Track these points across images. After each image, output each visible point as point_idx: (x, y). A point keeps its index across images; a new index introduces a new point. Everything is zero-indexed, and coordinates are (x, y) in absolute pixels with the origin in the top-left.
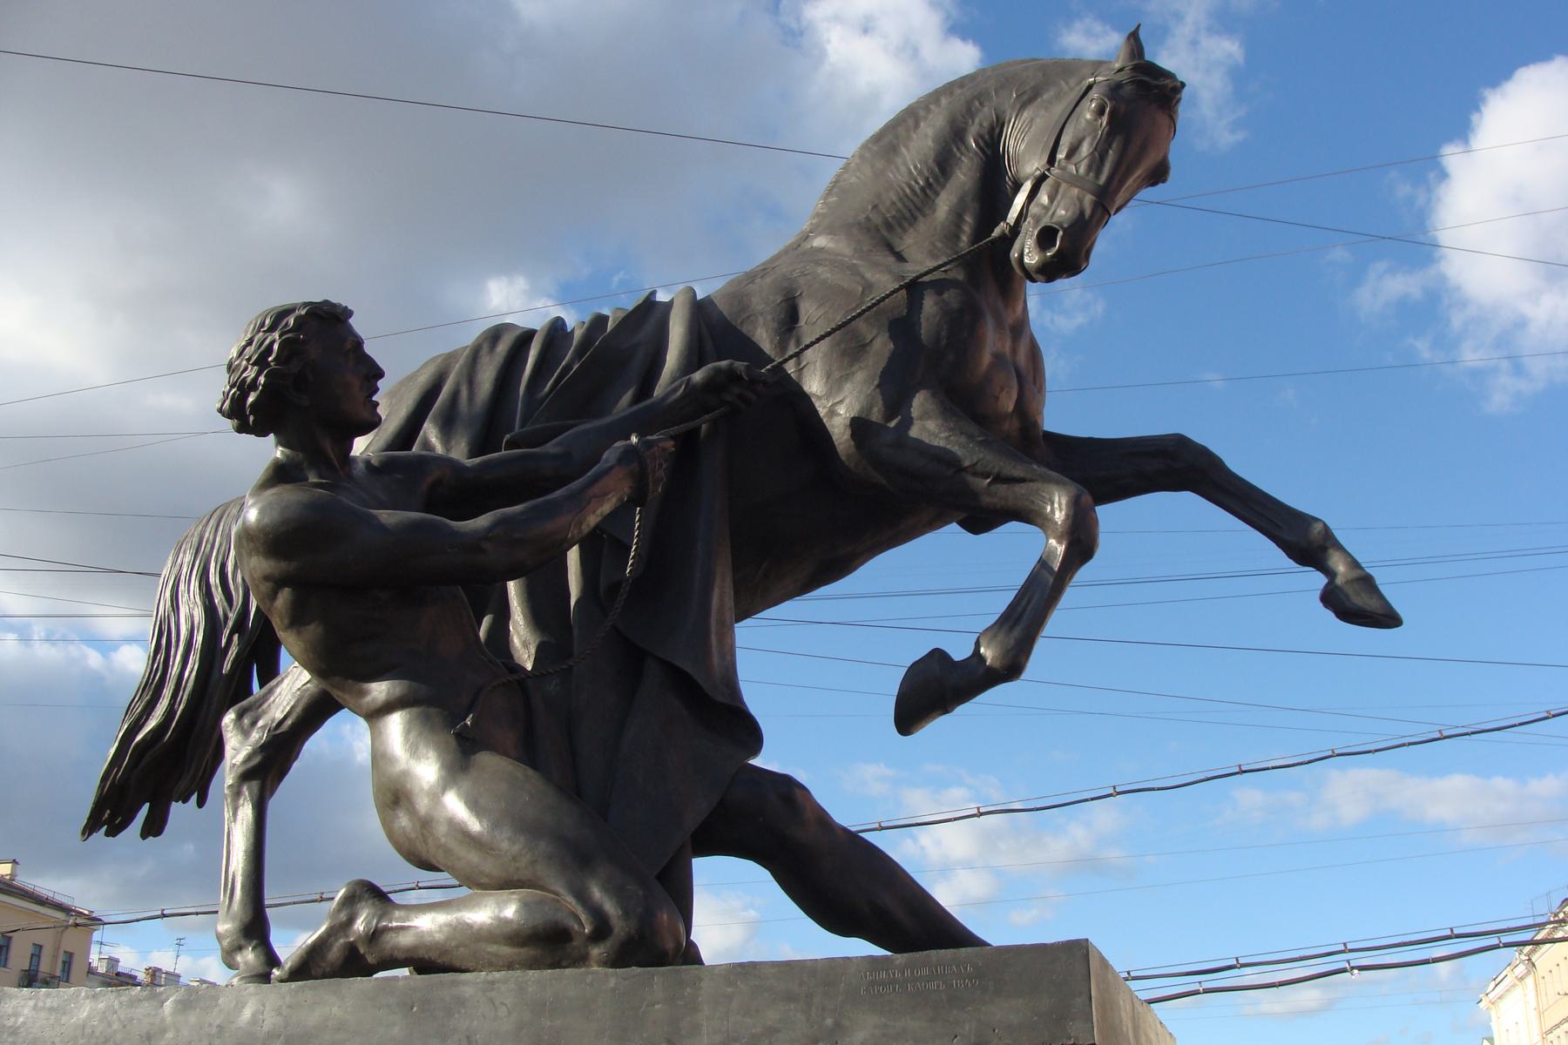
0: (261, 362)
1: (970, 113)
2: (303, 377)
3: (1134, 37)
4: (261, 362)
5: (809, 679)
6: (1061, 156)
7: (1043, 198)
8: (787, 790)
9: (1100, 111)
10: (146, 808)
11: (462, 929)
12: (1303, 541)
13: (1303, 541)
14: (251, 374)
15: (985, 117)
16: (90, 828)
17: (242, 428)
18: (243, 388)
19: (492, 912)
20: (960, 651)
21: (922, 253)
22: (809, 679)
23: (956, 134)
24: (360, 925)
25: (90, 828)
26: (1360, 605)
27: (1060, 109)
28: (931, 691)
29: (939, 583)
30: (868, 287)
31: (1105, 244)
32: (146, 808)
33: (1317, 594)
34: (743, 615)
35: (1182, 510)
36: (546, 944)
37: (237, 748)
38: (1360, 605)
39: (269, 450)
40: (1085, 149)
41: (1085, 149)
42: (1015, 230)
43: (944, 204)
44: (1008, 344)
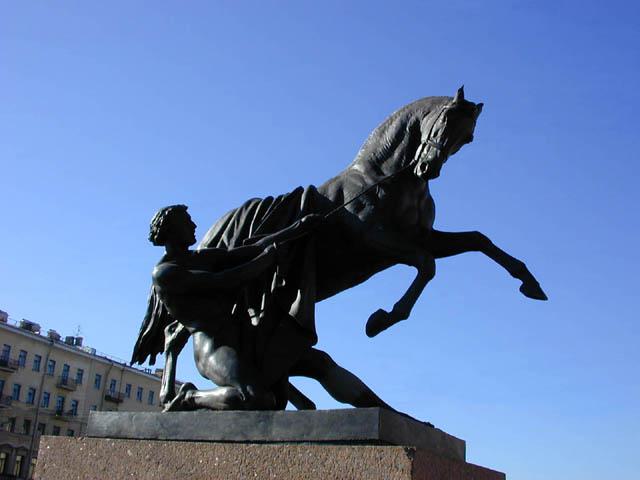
0: (158, 226)
1: (408, 118)
2: (174, 228)
3: (461, 91)
4: (158, 226)
5: (339, 323)
6: (432, 135)
7: (425, 151)
8: (323, 356)
9: (444, 121)
10: (149, 357)
11: (213, 397)
12: (516, 268)
13: (516, 268)
14: (155, 229)
15: (413, 118)
16: (482, 105)
17: (155, 245)
18: (154, 234)
19: (223, 392)
20: (389, 309)
21: (387, 169)
22: (339, 323)
23: (403, 126)
24: (187, 396)
25: (482, 105)
26: (532, 289)
27: (435, 116)
28: (378, 323)
29: (389, 284)
30: (365, 184)
31: (445, 168)
32: (149, 357)
33: (194, 383)
34: (318, 301)
35: (476, 258)
36: (232, 403)
37: (169, 339)
38: (532, 289)
39: (162, 251)
40: (440, 134)
41: (440, 134)
42: (417, 162)
43: (396, 154)
44: (416, 202)
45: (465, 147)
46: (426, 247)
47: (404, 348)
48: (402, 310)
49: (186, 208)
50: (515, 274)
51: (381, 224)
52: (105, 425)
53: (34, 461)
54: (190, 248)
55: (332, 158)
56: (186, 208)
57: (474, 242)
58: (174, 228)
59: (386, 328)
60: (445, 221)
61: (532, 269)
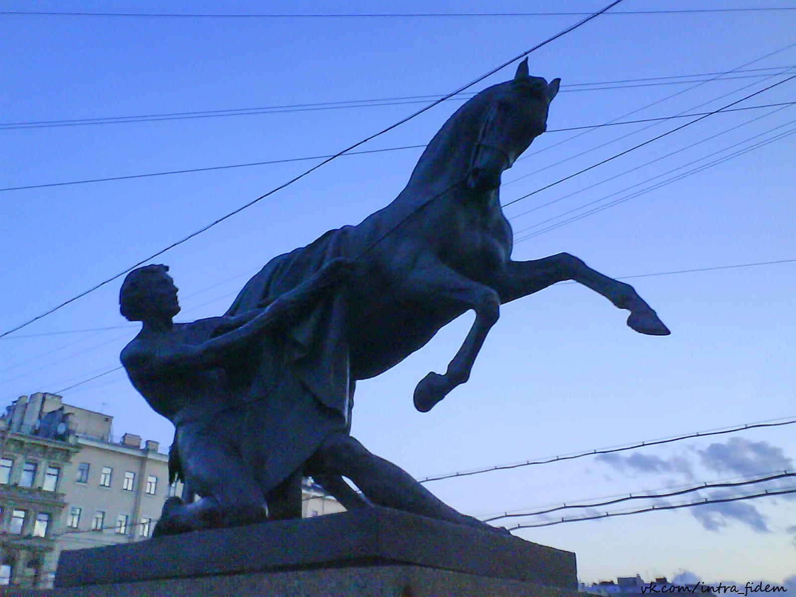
10: (345, 479)
12: (622, 295)
13: (622, 295)
26: (646, 321)
28: (429, 394)
35: (567, 291)
38: (646, 321)
45: (538, 141)
46: (492, 278)
47: (472, 429)
48: (460, 371)
49: (167, 268)
50: (620, 304)
51: (435, 259)
52: (46, 554)
53: (237, 575)
54: (176, 319)
55: (361, 182)
56: (167, 268)
57: (563, 268)
58: (147, 294)
59: (442, 398)
60: (524, 250)
61: (643, 292)
